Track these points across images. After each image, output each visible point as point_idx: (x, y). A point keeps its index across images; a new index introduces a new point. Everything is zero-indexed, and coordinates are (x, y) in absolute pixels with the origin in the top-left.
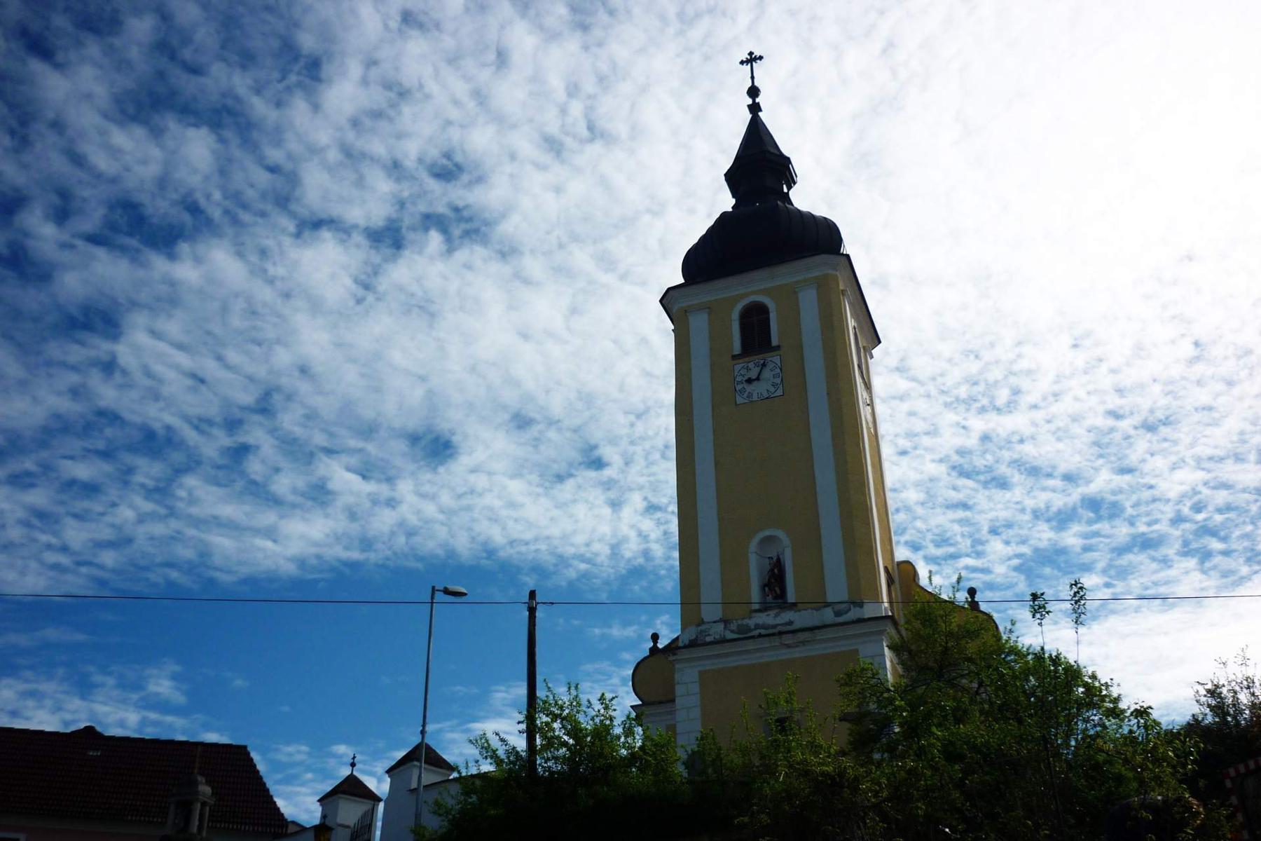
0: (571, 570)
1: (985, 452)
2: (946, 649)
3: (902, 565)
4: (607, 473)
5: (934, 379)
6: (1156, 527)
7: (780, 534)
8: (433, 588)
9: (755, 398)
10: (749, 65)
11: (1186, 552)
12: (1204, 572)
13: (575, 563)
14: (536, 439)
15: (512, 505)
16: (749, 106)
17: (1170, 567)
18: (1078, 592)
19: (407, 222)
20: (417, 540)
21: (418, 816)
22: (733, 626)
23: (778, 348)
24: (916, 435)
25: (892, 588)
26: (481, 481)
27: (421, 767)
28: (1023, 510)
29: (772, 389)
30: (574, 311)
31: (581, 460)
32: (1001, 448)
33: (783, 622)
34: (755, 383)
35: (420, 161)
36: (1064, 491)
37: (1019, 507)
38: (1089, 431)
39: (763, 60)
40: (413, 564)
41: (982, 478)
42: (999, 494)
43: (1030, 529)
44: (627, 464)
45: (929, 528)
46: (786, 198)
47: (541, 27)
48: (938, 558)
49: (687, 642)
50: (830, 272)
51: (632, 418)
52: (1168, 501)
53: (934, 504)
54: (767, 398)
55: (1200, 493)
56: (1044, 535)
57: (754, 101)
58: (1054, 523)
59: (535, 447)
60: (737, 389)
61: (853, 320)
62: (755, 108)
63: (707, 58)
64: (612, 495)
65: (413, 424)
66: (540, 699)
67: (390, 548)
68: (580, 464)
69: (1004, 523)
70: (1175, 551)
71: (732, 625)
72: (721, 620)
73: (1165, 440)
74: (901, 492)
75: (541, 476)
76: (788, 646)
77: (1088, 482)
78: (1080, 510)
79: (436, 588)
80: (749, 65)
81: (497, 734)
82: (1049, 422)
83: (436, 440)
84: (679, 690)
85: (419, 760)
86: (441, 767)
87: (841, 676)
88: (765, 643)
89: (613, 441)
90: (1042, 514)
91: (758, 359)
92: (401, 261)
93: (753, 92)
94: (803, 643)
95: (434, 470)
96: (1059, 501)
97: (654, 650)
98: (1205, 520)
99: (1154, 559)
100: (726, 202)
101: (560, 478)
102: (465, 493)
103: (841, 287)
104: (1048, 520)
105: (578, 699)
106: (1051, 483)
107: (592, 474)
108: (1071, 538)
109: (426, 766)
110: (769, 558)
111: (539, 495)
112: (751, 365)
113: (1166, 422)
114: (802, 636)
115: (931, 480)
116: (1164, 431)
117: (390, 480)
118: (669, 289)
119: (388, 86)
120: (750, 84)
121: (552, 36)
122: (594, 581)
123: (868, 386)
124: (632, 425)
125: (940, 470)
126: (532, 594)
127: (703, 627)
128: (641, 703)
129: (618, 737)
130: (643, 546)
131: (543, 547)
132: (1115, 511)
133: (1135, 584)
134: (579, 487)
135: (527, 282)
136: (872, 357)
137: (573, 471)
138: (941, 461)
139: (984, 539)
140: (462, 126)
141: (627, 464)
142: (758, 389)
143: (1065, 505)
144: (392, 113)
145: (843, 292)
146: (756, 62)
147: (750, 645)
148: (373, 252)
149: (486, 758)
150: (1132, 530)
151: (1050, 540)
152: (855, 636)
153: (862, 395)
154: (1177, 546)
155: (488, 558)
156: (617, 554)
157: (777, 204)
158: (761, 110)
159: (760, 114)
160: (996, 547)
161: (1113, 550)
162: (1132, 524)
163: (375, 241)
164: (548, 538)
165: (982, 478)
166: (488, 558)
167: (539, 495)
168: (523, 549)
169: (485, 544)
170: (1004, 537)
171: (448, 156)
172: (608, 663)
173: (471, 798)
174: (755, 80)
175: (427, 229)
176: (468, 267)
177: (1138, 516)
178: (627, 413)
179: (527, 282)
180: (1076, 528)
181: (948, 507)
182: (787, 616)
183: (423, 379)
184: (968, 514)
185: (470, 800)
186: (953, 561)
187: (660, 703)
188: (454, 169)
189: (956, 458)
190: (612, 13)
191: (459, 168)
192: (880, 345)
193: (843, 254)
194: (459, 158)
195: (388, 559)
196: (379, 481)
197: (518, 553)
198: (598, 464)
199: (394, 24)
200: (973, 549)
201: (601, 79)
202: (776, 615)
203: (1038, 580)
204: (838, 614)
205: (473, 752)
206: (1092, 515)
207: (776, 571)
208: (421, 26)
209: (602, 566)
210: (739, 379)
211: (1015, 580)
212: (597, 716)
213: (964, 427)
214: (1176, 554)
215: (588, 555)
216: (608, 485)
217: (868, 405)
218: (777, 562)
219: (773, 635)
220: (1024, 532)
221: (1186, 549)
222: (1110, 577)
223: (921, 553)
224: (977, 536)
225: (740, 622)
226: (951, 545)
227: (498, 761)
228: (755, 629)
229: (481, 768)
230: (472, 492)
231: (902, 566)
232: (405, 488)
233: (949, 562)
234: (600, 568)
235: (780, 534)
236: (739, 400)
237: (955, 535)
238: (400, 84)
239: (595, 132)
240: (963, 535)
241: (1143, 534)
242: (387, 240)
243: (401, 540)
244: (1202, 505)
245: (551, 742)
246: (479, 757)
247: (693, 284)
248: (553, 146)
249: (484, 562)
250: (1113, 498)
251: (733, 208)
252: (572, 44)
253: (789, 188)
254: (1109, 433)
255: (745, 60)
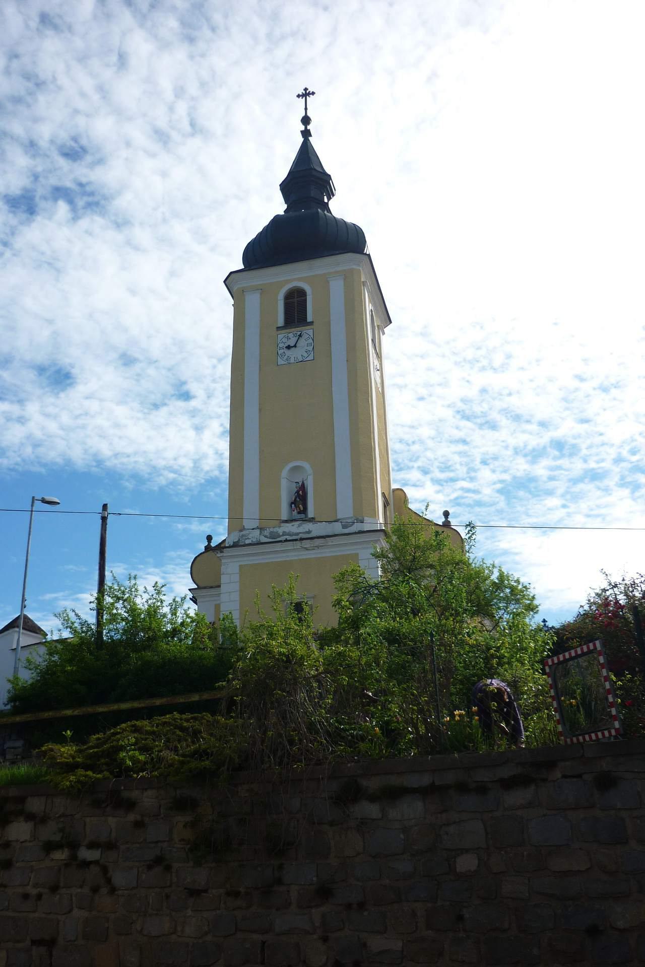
0: (161, 478)
1: (483, 401)
2: (414, 558)
3: (396, 492)
4: (193, 403)
5: (448, 343)
6: (602, 465)
7: (306, 466)
8: (33, 497)
9: (292, 361)
10: (304, 98)
11: (623, 483)
12: (634, 499)
13: (166, 473)
14: (138, 375)
15: (117, 425)
16: (302, 132)
17: (610, 494)
18: (471, 530)
19: (40, 192)
20: (41, 450)
21: (16, 670)
22: (267, 533)
23: (312, 323)
24: (432, 386)
25: (388, 508)
26: (94, 406)
27: (19, 632)
28: (507, 447)
29: (306, 355)
30: (173, 274)
31: (173, 392)
32: (494, 399)
33: (304, 531)
34: (293, 349)
35: (52, 142)
36: (538, 434)
37: (504, 444)
38: (560, 389)
39: (315, 95)
40: (36, 469)
41: (479, 421)
42: (489, 433)
43: (511, 462)
44: (209, 397)
45: (436, 457)
46: (326, 206)
47: (156, 37)
48: (441, 480)
49: (232, 544)
50: (354, 267)
51: (215, 361)
52: (613, 445)
53: (441, 439)
54: (301, 361)
55: (636, 440)
56: (521, 466)
57: (306, 128)
58: (529, 458)
59: (138, 380)
60: (279, 353)
61: (370, 305)
62: (306, 134)
63: (289, 74)
64: (197, 420)
65: (40, 358)
66: (107, 585)
67: (19, 456)
68: (172, 396)
69: (492, 456)
70: (614, 483)
71: (266, 532)
72: (258, 528)
73: (615, 399)
74: (417, 429)
75: (142, 403)
76: (307, 549)
77: (557, 428)
78: (549, 449)
79: (36, 498)
80: (304, 98)
81: (73, 611)
82: (531, 381)
83: (58, 372)
84: (224, 579)
85: (18, 627)
86: (37, 633)
87: (337, 575)
88: (289, 546)
89: (199, 379)
90: (521, 451)
91: (297, 330)
92: (34, 225)
93: (306, 120)
94: (318, 547)
95: (57, 395)
96: (534, 442)
97: (208, 548)
98: (638, 461)
99: (599, 488)
100: (279, 207)
101: (156, 406)
102: (81, 415)
103: (363, 280)
104: (525, 456)
105: (136, 586)
106: (528, 427)
107: (181, 404)
108: (541, 470)
109: (25, 632)
110: (296, 482)
111: (138, 419)
112: (291, 335)
113: (616, 386)
114: (318, 542)
115: (440, 421)
116: (614, 392)
117: (21, 402)
118: (231, 273)
119: (27, 76)
120: (304, 114)
121: (164, 46)
122: (180, 487)
123: (379, 356)
124: (214, 367)
125: (448, 413)
126: (105, 507)
127: (244, 533)
128: (197, 587)
129: (164, 616)
130: (219, 462)
131: (141, 460)
132: (574, 451)
133: (584, 505)
134: (171, 414)
135: (137, 248)
136: (384, 333)
137: (167, 401)
138: (449, 406)
139: (476, 468)
140: (88, 116)
141: (209, 397)
142: (294, 354)
143: (538, 445)
144: (29, 99)
145: (364, 283)
146: (309, 97)
147: (278, 547)
148: (11, 215)
149: (67, 627)
150: (585, 466)
151: (525, 470)
152: (356, 543)
153: (373, 363)
154: (617, 478)
155: (97, 466)
156: (198, 467)
157: (318, 212)
158: (311, 136)
159: (310, 138)
160: (485, 474)
161: (570, 480)
162: (585, 461)
163: (13, 206)
164: (145, 452)
165: (479, 421)
166: (97, 466)
167: (138, 419)
168: (125, 460)
169: (95, 455)
170: (492, 466)
171: (75, 139)
172: (188, 551)
173: (54, 657)
174: (308, 111)
175: (56, 200)
176: (89, 233)
177: (590, 455)
178: (210, 357)
179: (137, 248)
180: (545, 462)
181: (451, 442)
182: (308, 526)
183: (50, 322)
184: (466, 448)
185: (53, 659)
186: (452, 484)
187: (212, 587)
188: (79, 150)
189: (461, 406)
190: (213, 29)
191: (84, 150)
192: (391, 324)
193: (366, 254)
194: (84, 142)
195: (17, 464)
196: (12, 402)
197: (123, 464)
198: (186, 396)
199: (34, 24)
200: (468, 475)
201: (203, 85)
202: (299, 526)
203: (514, 500)
204: (344, 527)
205: (57, 623)
206: (557, 453)
207: (301, 492)
208: (56, 27)
209: (186, 476)
210: (281, 345)
211: (498, 499)
212: (150, 599)
213: (468, 381)
214: (615, 485)
215: (176, 467)
216: (193, 413)
217: (378, 370)
218: (301, 485)
219: (296, 540)
220: (507, 464)
221: (622, 482)
222: (566, 500)
223: (429, 476)
224: (472, 465)
225: (271, 530)
226: (452, 471)
227: (74, 631)
228: (283, 535)
229: (62, 635)
230: (86, 414)
231: (396, 492)
232: (32, 409)
233: (449, 484)
234: (184, 477)
235: (306, 466)
236: (281, 362)
237: (455, 464)
238: (37, 76)
239: (196, 128)
240: (461, 465)
241: (593, 469)
242: (23, 207)
243: (29, 450)
244: (636, 449)
245: (114, 618)
246: (61, 627)
247: (249, 270)
248: (162, 137)
249: (94, 469)
250: (574, 441)
251: (284, 212)
252: (180, 53)
253: (329, 199)
254: (574, 392)
255: (301, 94)
